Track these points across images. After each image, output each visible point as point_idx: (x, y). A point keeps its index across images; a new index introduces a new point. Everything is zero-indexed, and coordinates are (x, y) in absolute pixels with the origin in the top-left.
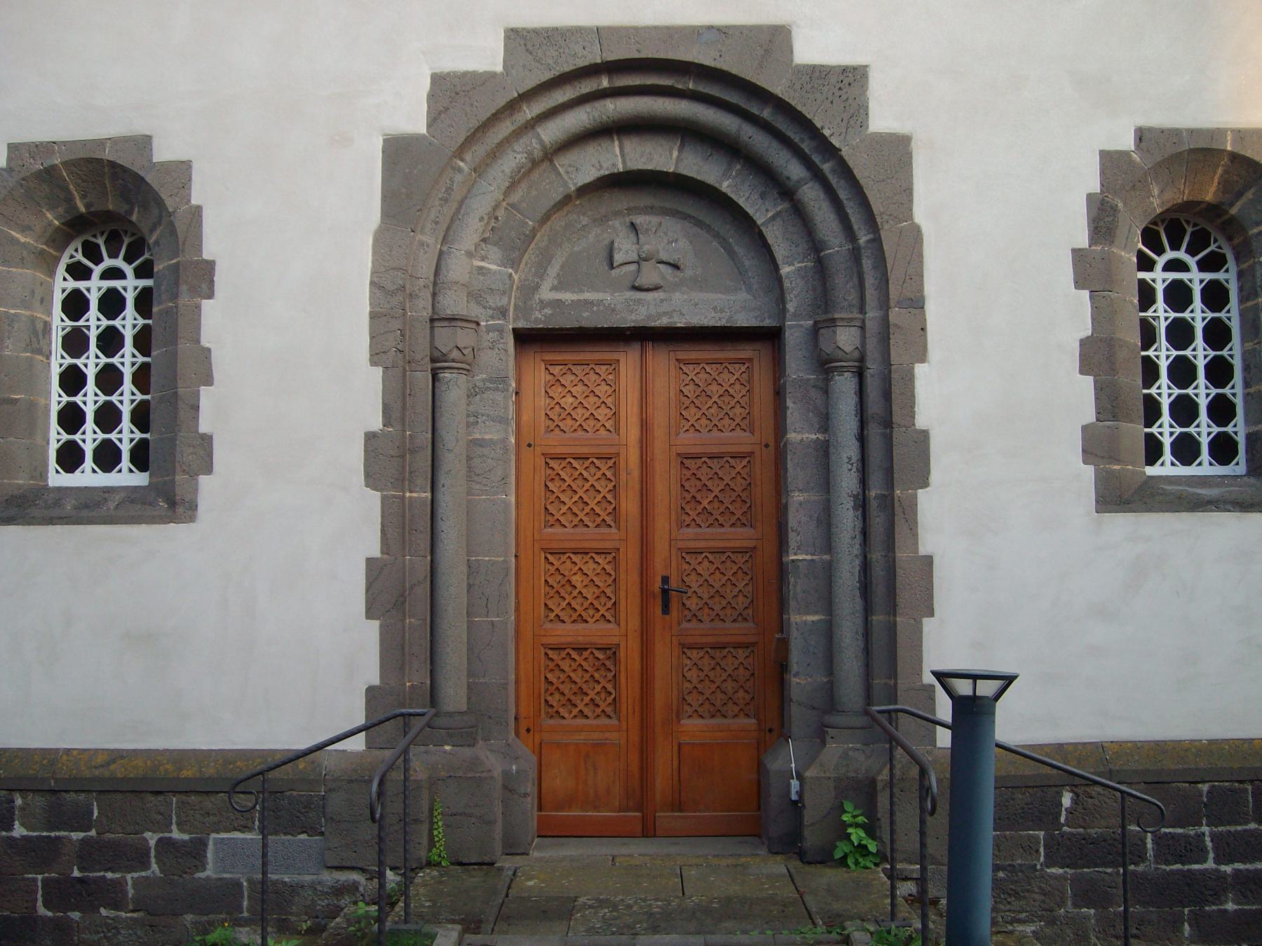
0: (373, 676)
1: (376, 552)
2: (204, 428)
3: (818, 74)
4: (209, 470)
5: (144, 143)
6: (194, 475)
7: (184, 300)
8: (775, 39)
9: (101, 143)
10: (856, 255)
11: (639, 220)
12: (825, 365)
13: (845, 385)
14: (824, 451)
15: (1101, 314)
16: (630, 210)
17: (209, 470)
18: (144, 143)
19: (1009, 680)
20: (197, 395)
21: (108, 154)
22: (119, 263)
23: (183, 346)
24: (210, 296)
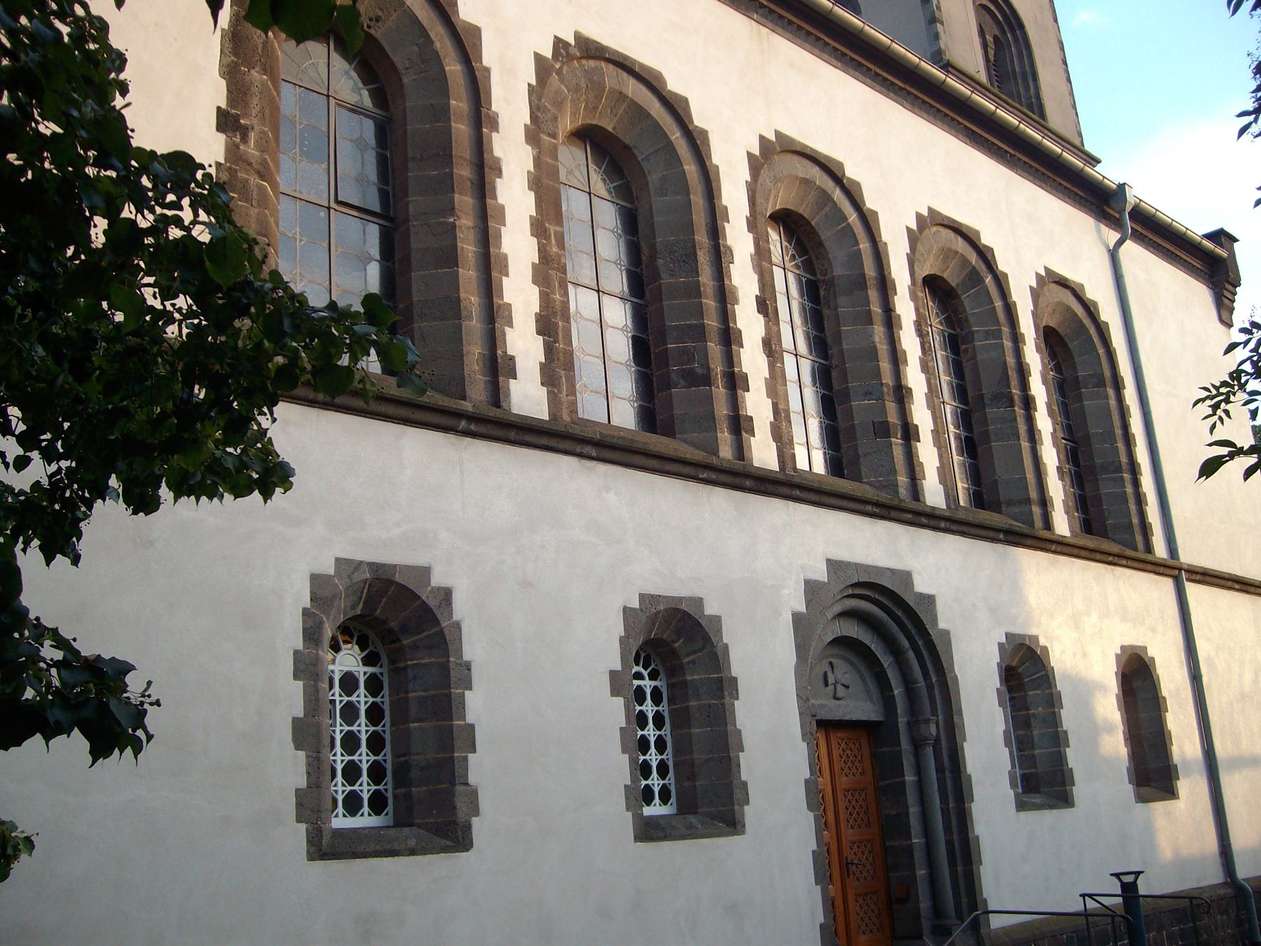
0: (820, 918)
1: (815, 848)
2: (743, 778)
3: (922, 596)
4: (748, 803)
5: (699, 602)
6: (742, 806)
7: (727, 699)
8: (906, 577)
9: (680, 599)
10: (930, 688)
11: (834, 661)
12: (917, 745)
13: (929, 751)
14: (921, 786)
15: (313, 700)
16: (832, 656)
17: (748, 803)
18: (699, 602)
19: (1138, 873)
20: (738, 757)
21: (684, 607)
22: (640, 669)
23: (730, 728)
24: (737, 698)
